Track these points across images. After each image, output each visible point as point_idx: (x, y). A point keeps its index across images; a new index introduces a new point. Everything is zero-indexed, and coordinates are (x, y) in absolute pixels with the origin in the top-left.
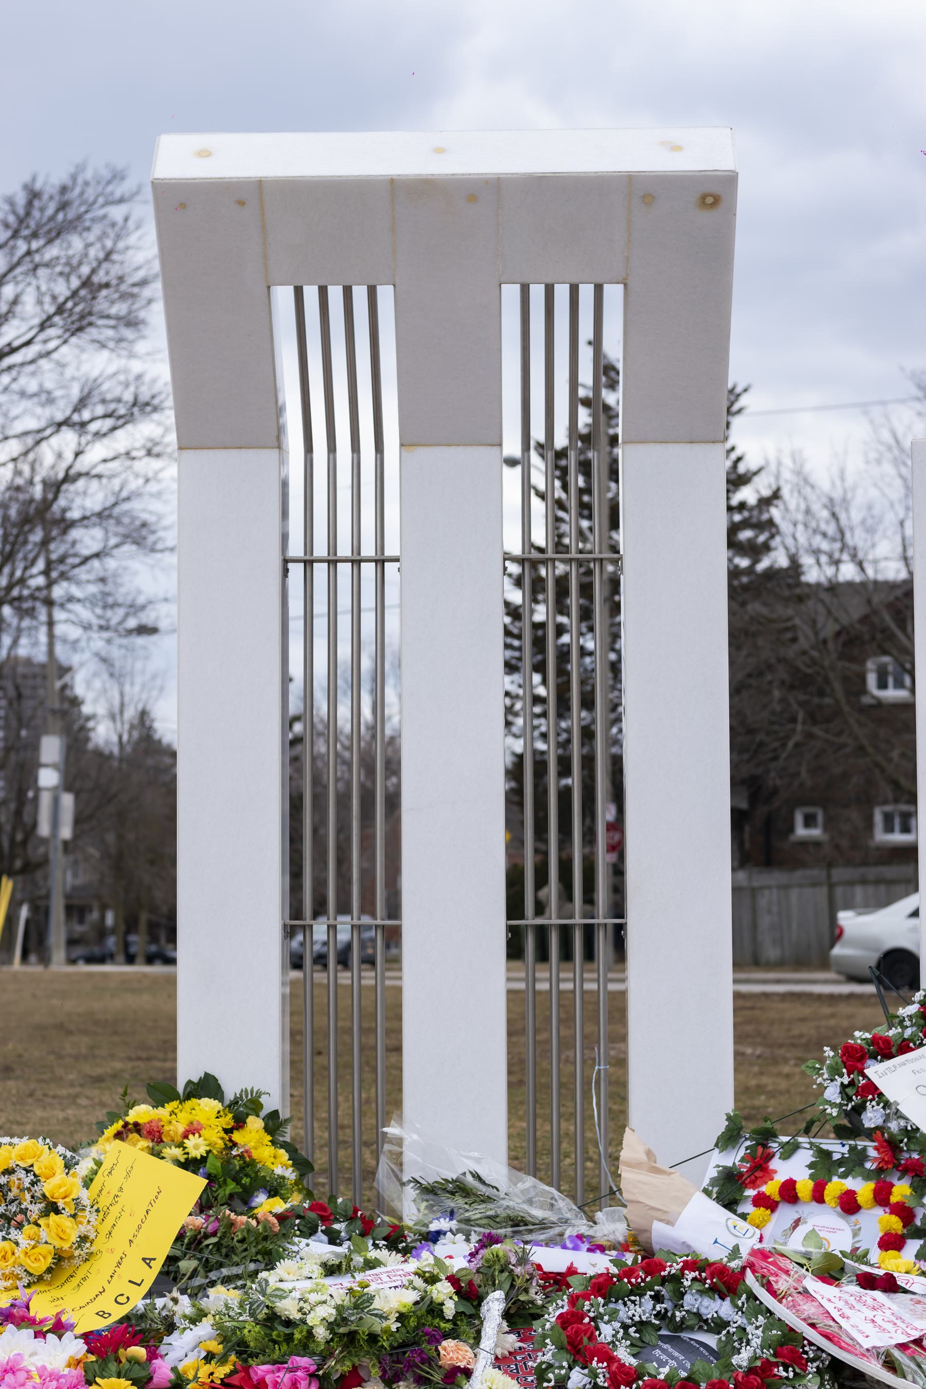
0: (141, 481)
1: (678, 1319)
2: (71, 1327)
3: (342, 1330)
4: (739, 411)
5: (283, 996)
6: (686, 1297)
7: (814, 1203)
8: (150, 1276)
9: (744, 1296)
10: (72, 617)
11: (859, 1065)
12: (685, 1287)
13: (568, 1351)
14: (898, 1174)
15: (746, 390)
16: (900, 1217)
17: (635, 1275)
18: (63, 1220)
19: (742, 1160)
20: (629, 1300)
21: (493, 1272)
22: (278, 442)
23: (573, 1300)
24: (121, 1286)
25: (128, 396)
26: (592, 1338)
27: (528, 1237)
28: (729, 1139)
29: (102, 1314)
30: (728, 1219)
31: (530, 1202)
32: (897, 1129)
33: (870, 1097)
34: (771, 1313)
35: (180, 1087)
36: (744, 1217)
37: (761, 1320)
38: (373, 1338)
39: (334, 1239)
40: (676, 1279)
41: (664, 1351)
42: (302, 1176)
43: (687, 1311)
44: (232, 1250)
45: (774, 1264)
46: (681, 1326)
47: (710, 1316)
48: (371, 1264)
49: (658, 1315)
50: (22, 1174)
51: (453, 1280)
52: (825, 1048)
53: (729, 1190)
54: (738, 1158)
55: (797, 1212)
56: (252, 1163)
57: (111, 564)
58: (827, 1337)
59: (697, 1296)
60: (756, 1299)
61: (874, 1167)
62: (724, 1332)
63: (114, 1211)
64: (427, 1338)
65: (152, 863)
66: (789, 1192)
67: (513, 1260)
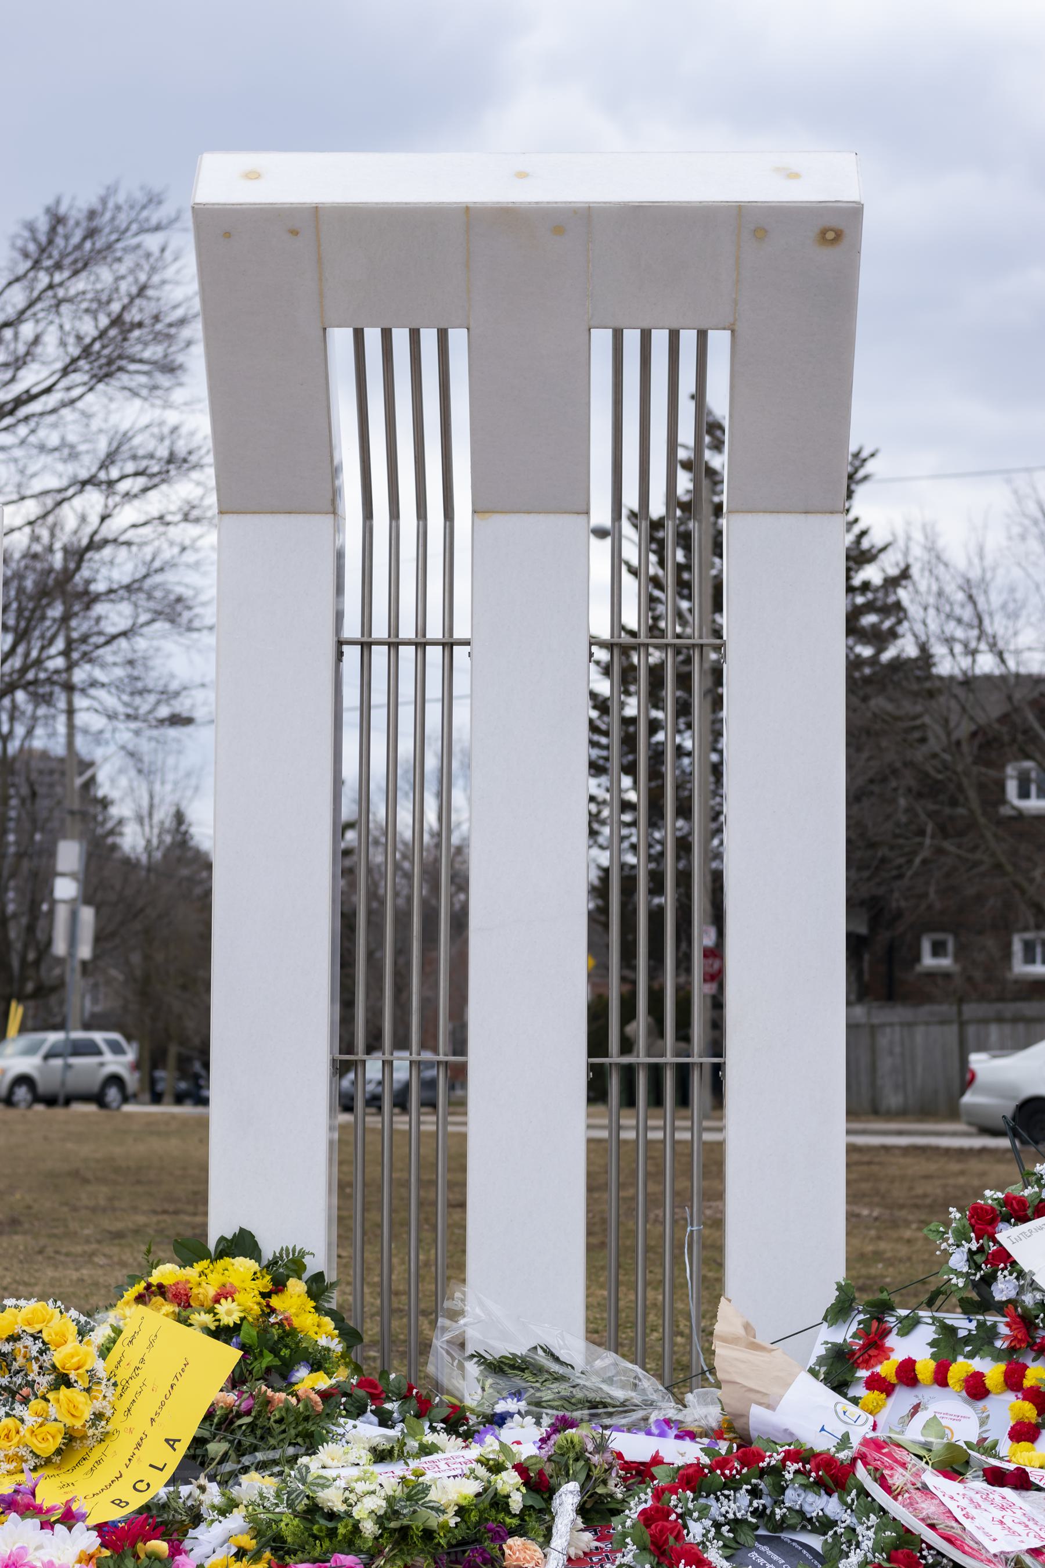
0: (176, 550)
1: (778, 1517)
2: (83, 1517)
3: (393, 1525)
4: (866, 478)
5: (331, 1143)
6: (787, 1492)
7: (936, 1387)
8: (174, 1459)
9: (854, 1492)
10: (96, 705)
11: (989, 1229)
12: (786, 1481)
13: (651, 1552)
14: (1033, 1354)
15: (873, 455)
16: (1034, 1404)
17: (730, 1466)
18: (74, 1395)
19: (854, 1336)
20: (723, 1494)
21: (567, 1461)
22: (333, 507)
23: (658, 1494)
24: (140, 1470)
25: (163, 452)
26: (679, 1537)
27: (607, 1421)
28: (838, 1312)
29: (119, 1503)
30: (836, 1404)
31: (610, 1381)
32: (1032, 1303)
33: (1002, 1265)
34: (885, 1512)
35: (212, 1245)
36: (855, 1401)
37: (873, 1519)
38: (428, 1534)
39: (385, 1420)
40: (776, 1471)
41: (762, 1554)
42: (349, 1347)
43: (789, 1509)
44: (269, 1431)
45: (889, 1455)
46: (782, 1526)
47: (814, 1514)
48: (426, 1450)
49: (755, 1513)
50: (29, 1341)
51: (521, 1469)
52: (951, 1209)
53: (838, 1371)
54: (850, 1333)
55: (917, 1396)
56: (293, 1332)
57: (141, 643)
58: (948, 1539)
59: (800, 1491)
60: (868, 1495)
61: (1005, 1346)
62: (831, 1533)
63: (134, 1385)
64: (490, 1535)
65: (184, 987)
66: (907, 1373)
67: (590, 1447)
